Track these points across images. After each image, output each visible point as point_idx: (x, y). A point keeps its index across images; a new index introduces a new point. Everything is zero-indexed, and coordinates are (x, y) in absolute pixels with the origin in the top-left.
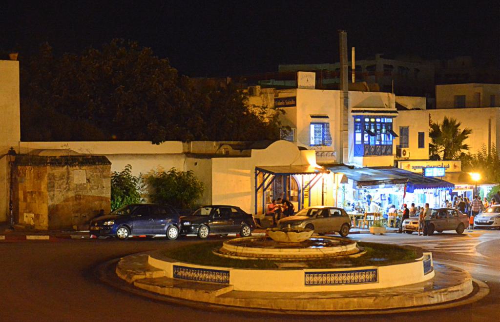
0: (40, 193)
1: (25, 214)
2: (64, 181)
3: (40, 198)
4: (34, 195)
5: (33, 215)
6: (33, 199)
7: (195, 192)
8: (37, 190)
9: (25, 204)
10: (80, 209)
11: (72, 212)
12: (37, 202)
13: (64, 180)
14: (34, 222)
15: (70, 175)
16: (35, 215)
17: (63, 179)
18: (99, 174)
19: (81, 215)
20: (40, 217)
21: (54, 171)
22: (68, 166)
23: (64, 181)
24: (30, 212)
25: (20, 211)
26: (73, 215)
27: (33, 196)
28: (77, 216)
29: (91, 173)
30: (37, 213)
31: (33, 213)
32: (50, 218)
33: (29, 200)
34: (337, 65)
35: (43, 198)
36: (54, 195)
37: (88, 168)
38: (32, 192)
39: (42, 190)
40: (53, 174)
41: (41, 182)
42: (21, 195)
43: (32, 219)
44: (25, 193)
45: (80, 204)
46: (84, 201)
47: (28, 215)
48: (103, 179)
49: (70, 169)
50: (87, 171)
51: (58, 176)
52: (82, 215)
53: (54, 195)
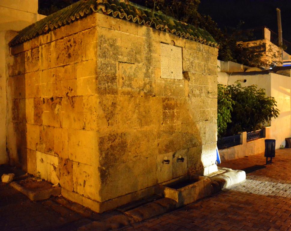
0: (72, 100)
1: (39, 155)
2: (140, 69)
3: (72, 116)
4: (58, 106)
5: (55, 160)
6: (55, 117)
7: (104, 113)
8: (64, 94)
9: (37, 129)
10: (172, 142)
11: (157, 152)
12: (65, 124)
13: (141, 65)
14: (59, 177)
15: (153, 55)
16: (61, 159)
17: (137, 60)
18: (203, 63)
19: (174, 156)
20: (75, 166)
21: (115, 33)
22: (148, 30)
23: (140, 69)
24: (49, 150)
25: (29, 146)
26: (160, 158)
27: (56, 111)
28: (168, 161)
29: (191, 59)
30: (65, 157)
31: (57, 154)
32: (104, 175)
33: (45, 120)
34: (262, 42)
35: (81, 113)
36: (114, 104)
37: (187, 45)
38: (52, 99)
39: (80, 92)
40: (115, 41)
41: (74, 70)
42: (30, 110)
43: (55, 168)
44: (37, 106)
45: (171, 130)
46: (179, 123)
47: (44, 156)
48: (209, 77)
49: (155, 37)
50: (185, 51)
51: (123, 50)
52: (176, 156)
53: (114, 104)
